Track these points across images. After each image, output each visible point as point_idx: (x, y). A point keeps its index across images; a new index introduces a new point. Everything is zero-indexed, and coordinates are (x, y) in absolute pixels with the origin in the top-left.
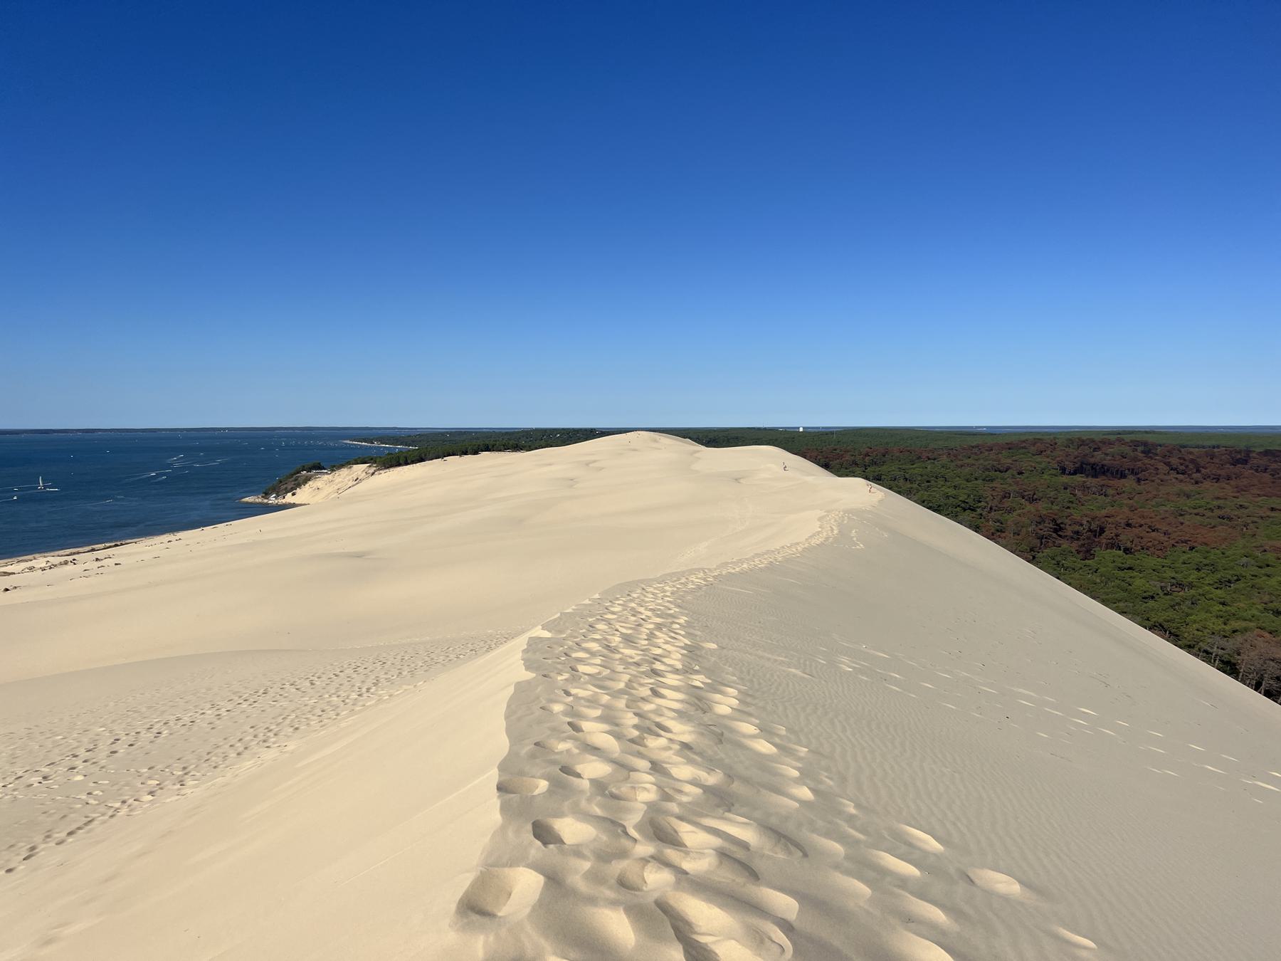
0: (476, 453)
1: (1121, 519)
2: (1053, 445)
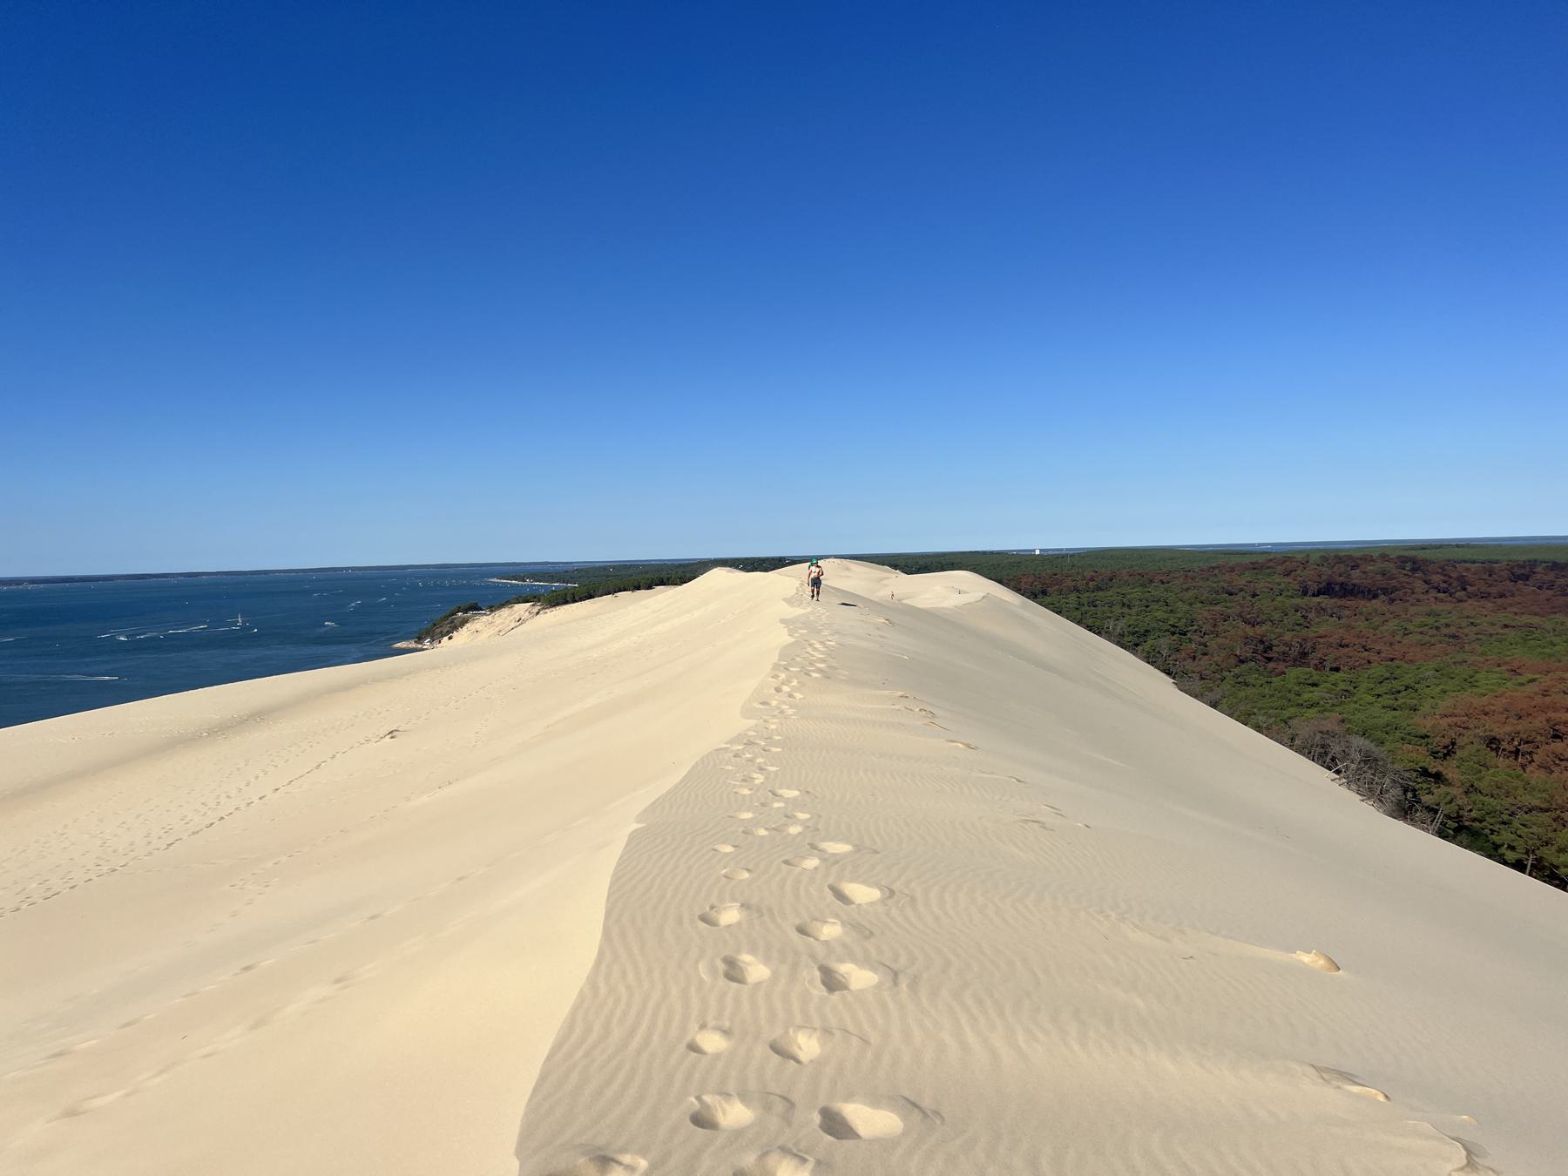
0: (650, 587)
1: (1334, 640)
2: (1305, 564)
